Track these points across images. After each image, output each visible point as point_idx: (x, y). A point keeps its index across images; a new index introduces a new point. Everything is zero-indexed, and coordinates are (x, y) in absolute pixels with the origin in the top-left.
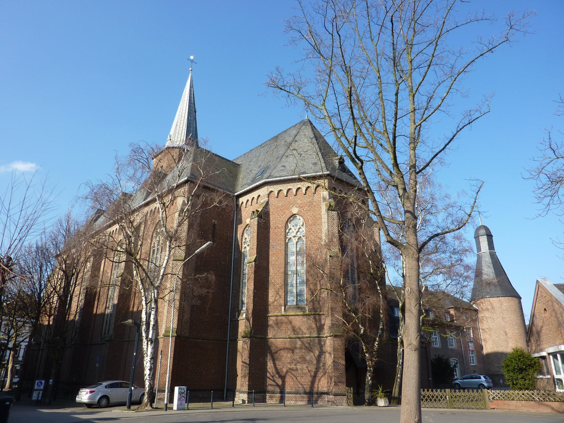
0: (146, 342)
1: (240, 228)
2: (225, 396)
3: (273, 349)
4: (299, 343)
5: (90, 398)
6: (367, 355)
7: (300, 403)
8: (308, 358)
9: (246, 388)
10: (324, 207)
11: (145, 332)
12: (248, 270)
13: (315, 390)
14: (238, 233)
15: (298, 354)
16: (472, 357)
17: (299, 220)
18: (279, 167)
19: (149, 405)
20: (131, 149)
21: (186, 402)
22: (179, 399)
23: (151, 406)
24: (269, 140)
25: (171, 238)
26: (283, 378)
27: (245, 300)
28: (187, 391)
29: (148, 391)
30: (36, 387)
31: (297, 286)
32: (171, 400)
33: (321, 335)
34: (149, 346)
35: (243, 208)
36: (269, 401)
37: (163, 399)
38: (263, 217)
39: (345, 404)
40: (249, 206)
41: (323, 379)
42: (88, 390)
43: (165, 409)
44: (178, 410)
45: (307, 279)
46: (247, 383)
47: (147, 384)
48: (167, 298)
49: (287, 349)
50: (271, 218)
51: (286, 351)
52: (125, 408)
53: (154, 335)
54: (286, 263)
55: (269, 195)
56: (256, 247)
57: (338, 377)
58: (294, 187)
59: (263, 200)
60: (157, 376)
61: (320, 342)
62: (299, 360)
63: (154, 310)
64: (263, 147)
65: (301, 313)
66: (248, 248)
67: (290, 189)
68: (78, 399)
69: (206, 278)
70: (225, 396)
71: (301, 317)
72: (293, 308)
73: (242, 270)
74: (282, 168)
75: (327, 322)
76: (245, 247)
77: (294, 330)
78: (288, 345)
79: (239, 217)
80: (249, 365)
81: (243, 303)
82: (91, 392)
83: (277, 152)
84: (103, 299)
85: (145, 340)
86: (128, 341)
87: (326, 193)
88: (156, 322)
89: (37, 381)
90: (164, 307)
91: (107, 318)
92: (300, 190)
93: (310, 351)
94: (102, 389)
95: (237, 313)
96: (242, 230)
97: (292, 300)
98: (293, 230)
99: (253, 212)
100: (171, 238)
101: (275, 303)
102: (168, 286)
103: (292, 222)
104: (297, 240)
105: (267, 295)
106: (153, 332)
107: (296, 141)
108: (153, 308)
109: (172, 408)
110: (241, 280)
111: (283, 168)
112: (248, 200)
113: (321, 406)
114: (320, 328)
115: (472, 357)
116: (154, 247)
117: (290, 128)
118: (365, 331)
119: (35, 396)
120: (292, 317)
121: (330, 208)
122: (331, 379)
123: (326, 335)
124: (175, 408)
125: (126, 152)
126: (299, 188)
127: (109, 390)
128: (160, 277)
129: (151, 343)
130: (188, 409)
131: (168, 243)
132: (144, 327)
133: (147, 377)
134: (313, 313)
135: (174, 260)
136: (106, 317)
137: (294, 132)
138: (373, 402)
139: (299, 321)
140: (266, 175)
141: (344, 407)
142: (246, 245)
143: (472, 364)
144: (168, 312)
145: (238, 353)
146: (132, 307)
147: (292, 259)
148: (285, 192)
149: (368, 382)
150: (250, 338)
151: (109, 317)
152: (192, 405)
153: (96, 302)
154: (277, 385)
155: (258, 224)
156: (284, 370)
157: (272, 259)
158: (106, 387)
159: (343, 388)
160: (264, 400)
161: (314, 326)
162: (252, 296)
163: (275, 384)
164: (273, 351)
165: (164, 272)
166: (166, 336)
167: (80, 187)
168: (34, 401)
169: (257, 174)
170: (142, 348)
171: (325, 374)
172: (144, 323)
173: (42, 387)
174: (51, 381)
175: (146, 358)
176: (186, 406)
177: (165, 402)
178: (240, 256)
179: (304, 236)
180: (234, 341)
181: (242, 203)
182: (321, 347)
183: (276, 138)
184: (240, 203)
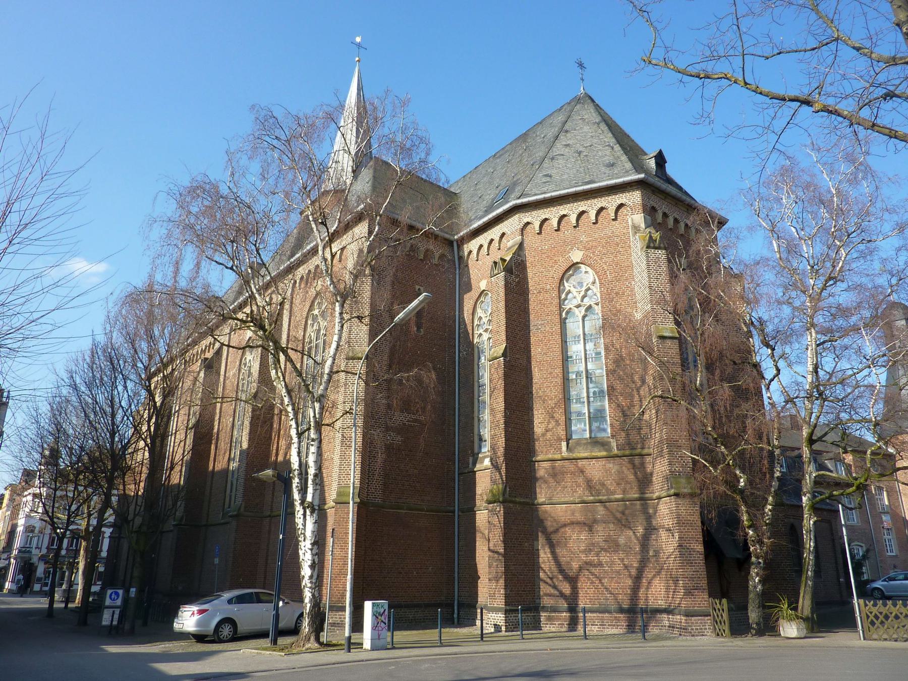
0: (302, 512)
1: (468, 301)
2: (455, 616)
3: (548, 524)
4: (601, 510)
5: (199, 624)
6: (751, 532)
7: (614, 631)
8: (622, 540)
9: (500, 602)
10: (637, 245)
11: (299, 491)
12: (489, 374)
13: (641, 604)
14: (465, 309)
15: (600, 534)
16: (890, 540)
17: (587, 275)
18: (539, 177)
19: (312, 638)
20: (253, 117)
21: (389, 630)
22: (374, 628)
23: (317, 639)
24: (511, 144)
25: (344, 298)
26: (573, 581)
27: (486, 433)
28: (390, 607)
29: (311, 611)
30: (108, 602)
31: (589, 402)
32: (357, 626)
33: (647, 495)
34: (308, 517)
35: (471, 262)
36: (547, 628)
37: (341, 625)
38: (515, 272)
39: (709, 632)
40: (483, 260)
41: (656, 582)
42: (195, 608)
43: (346, 647)
44: (373, 649)
45: (611, 388)
46: (502, 591)
47: (308, 595)
48: (338, 424)
49: (578, 523)
50: (530, 274)
51: (577, 528)
52: (266, 643)
53: (317, 497)
54: (566, 359)
55: (522, 230)
56: (504, 328)
57: (692, 579)
58: (571, 210)
59: (512, 242)
60: (327, 580)
61: (645, 508)
62: (603, 544)
63: (315, 443)
64: (499, 157)
65: (604, 453)
66: (485, 336)
67: (564, 216)
68: (177, 626)
69: (419, 380)
70: (455, 616)
71: (602, 462)
72: (585, 444)
73: (476, 379)
74: (544, 180)
75: (659, 468)
76: (481, 335)
77: (590, 485)
78: (579, 517)
79: (465, 279)
80: (505, 555)
81: (481, 439)
82: (201, 612)
83: (530, 156)
84: (223, 445)
85: (299, 509)
86: (270, 516)
87: (639, 218)
88: (319, 468)
89: (109, 592)
90: (333, 440)
91: (233, 477)
92: (584, 216)
93: (625, 526)
94: (221, 606)
95: (471, 459)
96: (472, 302)
97: (581, 429)
98: (575, 294)
99: (495, 263)
100: (344, 298)
101: (549, 435)
102: (341, 399)
103: (572, 280)
104: (583, 312)
105: (531, 422)
106: (315, 490)
107: (567, 131)
108: (313, 440)
109: (360, 645)
110: (476, 396)
111: (548, 179)
112: (481, 246)
113: (658, 638)
114: (645, 481)
115: (890, 540)
116: (310, 342)
117: (551, 115)
118: (750, 482)
119: (106, 618)
120: (584, 462)
121: (651, 245)
122: (676, 581)
123: (657, 494)
124: (367, 645)
125: (246, 125)
126: (583, 212)
127: (235, 608)
128: (326, 377)
129: (312, 512)
130: (394, 648)
131: (337, 309)
132: (296, 481)
133: (306, 582)
134: (627, 452)
135: (348, 358)
136: (230, 475)
137: (561, 118)
138: (768, 627)
139: (596, 470)
140: (518, 190)
141: (708, 639)
142: (481, 331)
143: (889, 554)
144: (343, 457)
145: (478, 535)
146: (274, 455)
147: (576, 349)
148: (554, 222)
149: (755, 587)
150: (503, 502)
151: (236, 476)
152: (401, 636)
153: (213, 447)
154: (562, 595)
155: (506, 285)
156: (575, 565)
157: (536, 351)
158: (230, 601)
159: (702, 600)
160: (536, 625)
161: (631, 477)
162: (502, 421)
163: (556, 592)
164: (550, 529)
165: (332, 366)
166: (341, 502)
167: (155, 198)
168: (105, 626)
169: (493, 199)
170: (294, 523)
171: (659, 573)
172: (296, 473)
173: (119, 602)
174: (133, 590)
175: (302, 544)
176: (389, 639)
177: (347, 635)
178: (471, 352)
179: (597, 304)
180: (470, 511)
181: (470, 252)
182: (649, 518)
183: (524, 137)
184: (466, 254)
